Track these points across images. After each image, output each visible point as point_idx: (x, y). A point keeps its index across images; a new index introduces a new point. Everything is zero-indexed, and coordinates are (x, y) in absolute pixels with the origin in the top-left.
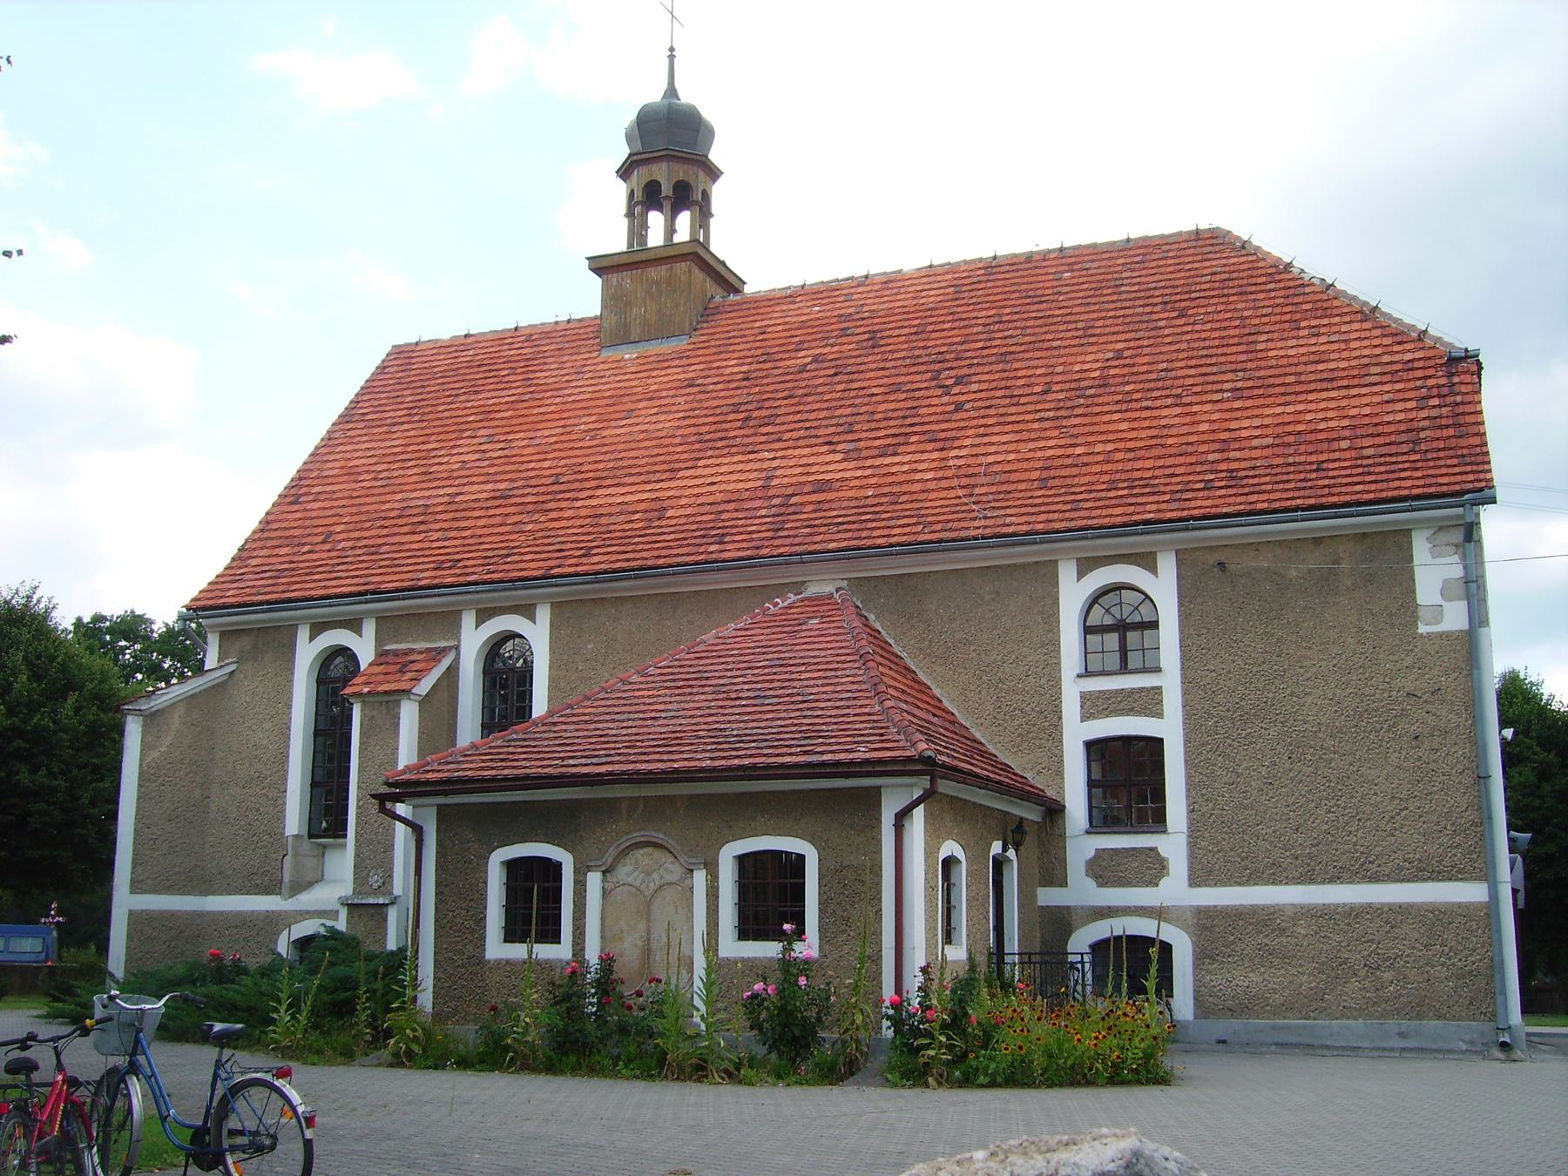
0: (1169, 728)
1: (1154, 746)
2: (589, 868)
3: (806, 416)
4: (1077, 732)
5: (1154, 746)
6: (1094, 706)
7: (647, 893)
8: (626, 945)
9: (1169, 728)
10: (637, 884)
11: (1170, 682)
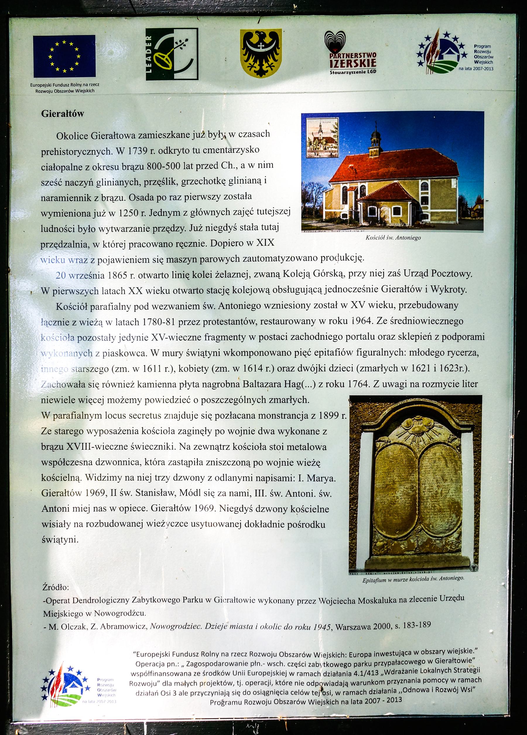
0: (429, 196)
1: (428, 197)
2: (364, 429)
3: (127, 424)
4: (420, 196)
5: (428, 197)
6: (422, 193)
7: (417, 450)
8: (398, 494)
9: (429, 196)
10: (408, 443)
11: (429, 191)
